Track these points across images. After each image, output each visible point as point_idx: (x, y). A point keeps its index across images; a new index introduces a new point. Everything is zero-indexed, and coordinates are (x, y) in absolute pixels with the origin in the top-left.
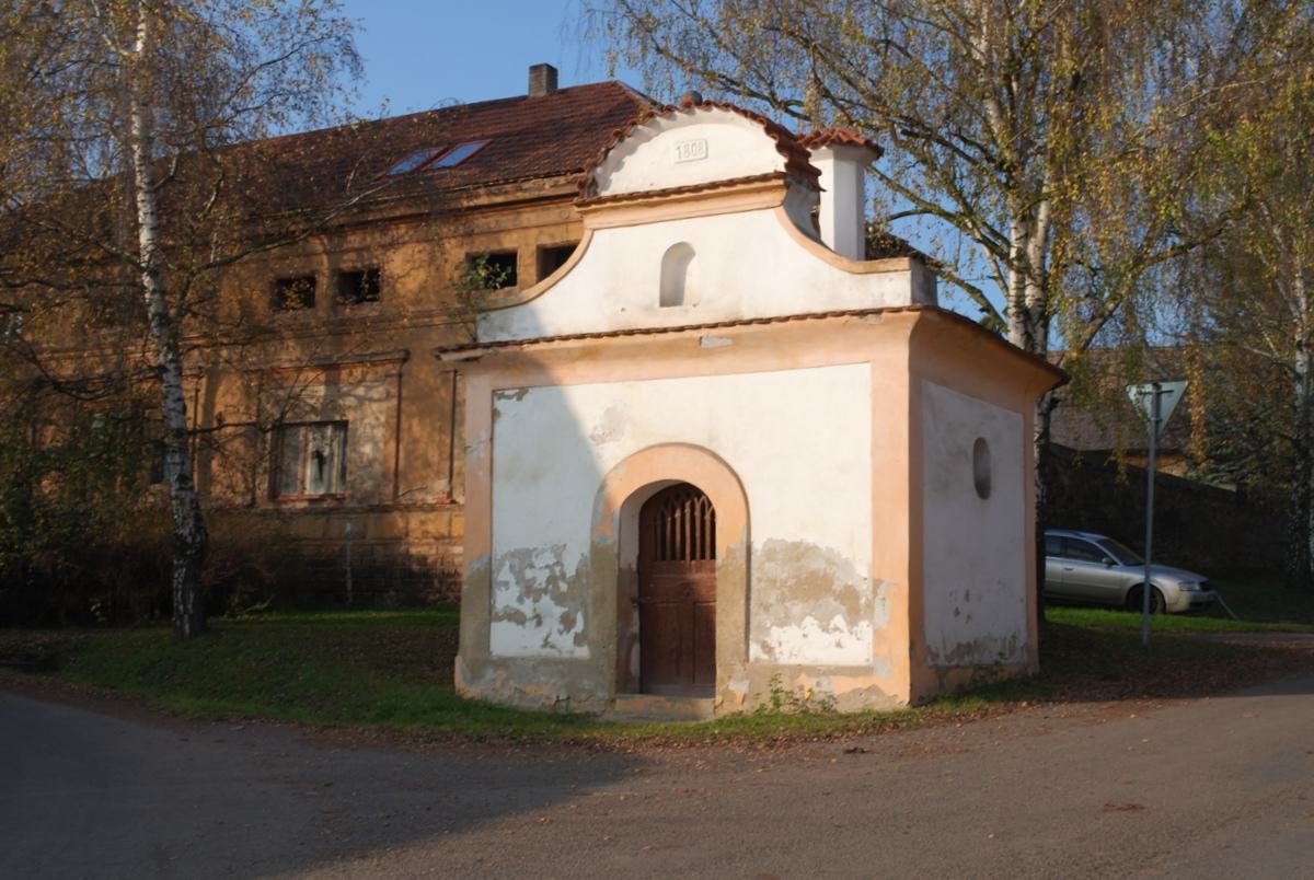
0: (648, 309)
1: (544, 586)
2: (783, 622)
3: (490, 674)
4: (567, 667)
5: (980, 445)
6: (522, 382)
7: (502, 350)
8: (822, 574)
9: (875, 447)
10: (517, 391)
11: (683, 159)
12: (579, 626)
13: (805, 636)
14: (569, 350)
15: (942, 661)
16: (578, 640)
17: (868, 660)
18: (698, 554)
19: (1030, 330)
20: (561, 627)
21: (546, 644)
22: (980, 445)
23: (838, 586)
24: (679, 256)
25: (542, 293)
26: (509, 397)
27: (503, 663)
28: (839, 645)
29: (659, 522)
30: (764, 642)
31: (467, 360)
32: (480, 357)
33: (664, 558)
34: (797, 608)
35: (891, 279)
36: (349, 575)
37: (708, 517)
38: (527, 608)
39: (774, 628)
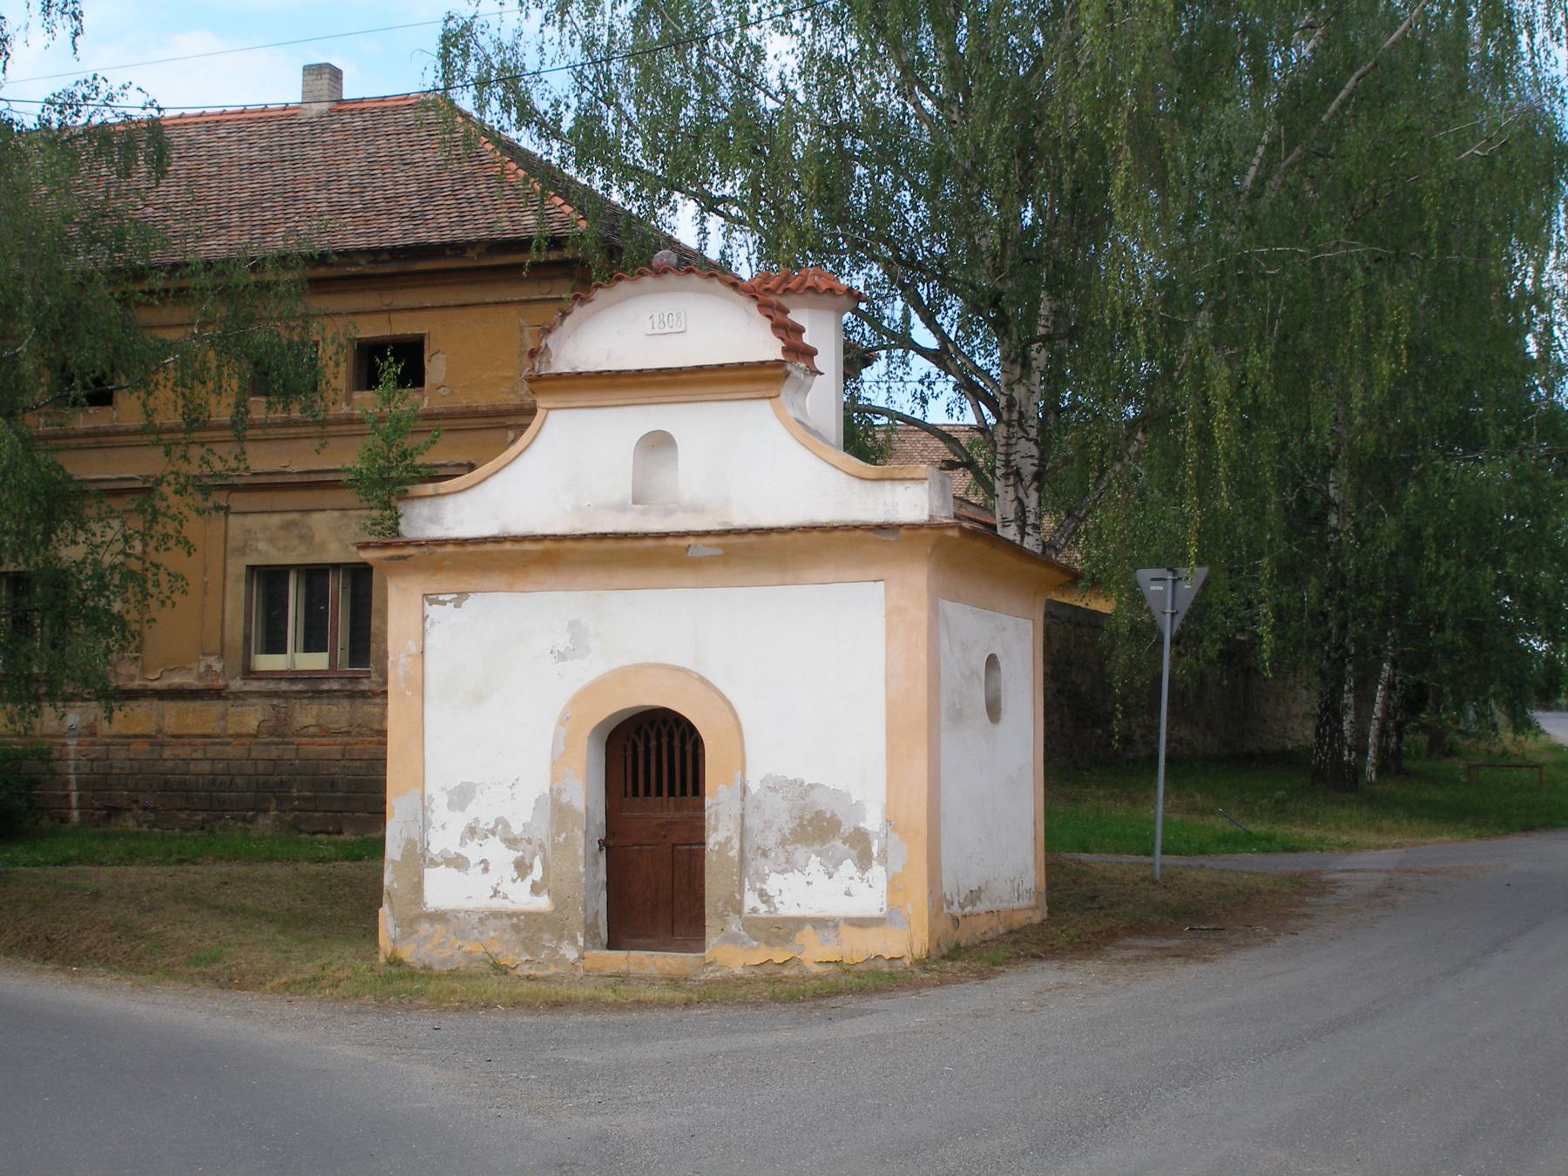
0: (621, 508)
1: (491, 826)
2: (788, 866)
3: (424, 928)
4: (527, 926)
5: (992, 662)
6: (461, 587)
7: (440, 550)
10: (456, 596)
11: (657, 331)
14: (525, 553)
15: (956, 909)
16: (536, 889)
17: (881, 909)
19: (1021, 495)
20: (515, 875)
21: (496, 893)
22: (992, 662)
23: (847, 828)
24: (658, 443)
25: (484, 480)
26: (443, 603)
27: (439, 917)
28: (848, 894)
29: (630, 753)
30: (762, 890)
31: (391, 558)
32: (411, 556)
33: (635, 794)
34: (800, 852)
35: (906, 488)
36: (73, 786)
37: (689, 747)
38: (472, 851)
39: (773, 874)
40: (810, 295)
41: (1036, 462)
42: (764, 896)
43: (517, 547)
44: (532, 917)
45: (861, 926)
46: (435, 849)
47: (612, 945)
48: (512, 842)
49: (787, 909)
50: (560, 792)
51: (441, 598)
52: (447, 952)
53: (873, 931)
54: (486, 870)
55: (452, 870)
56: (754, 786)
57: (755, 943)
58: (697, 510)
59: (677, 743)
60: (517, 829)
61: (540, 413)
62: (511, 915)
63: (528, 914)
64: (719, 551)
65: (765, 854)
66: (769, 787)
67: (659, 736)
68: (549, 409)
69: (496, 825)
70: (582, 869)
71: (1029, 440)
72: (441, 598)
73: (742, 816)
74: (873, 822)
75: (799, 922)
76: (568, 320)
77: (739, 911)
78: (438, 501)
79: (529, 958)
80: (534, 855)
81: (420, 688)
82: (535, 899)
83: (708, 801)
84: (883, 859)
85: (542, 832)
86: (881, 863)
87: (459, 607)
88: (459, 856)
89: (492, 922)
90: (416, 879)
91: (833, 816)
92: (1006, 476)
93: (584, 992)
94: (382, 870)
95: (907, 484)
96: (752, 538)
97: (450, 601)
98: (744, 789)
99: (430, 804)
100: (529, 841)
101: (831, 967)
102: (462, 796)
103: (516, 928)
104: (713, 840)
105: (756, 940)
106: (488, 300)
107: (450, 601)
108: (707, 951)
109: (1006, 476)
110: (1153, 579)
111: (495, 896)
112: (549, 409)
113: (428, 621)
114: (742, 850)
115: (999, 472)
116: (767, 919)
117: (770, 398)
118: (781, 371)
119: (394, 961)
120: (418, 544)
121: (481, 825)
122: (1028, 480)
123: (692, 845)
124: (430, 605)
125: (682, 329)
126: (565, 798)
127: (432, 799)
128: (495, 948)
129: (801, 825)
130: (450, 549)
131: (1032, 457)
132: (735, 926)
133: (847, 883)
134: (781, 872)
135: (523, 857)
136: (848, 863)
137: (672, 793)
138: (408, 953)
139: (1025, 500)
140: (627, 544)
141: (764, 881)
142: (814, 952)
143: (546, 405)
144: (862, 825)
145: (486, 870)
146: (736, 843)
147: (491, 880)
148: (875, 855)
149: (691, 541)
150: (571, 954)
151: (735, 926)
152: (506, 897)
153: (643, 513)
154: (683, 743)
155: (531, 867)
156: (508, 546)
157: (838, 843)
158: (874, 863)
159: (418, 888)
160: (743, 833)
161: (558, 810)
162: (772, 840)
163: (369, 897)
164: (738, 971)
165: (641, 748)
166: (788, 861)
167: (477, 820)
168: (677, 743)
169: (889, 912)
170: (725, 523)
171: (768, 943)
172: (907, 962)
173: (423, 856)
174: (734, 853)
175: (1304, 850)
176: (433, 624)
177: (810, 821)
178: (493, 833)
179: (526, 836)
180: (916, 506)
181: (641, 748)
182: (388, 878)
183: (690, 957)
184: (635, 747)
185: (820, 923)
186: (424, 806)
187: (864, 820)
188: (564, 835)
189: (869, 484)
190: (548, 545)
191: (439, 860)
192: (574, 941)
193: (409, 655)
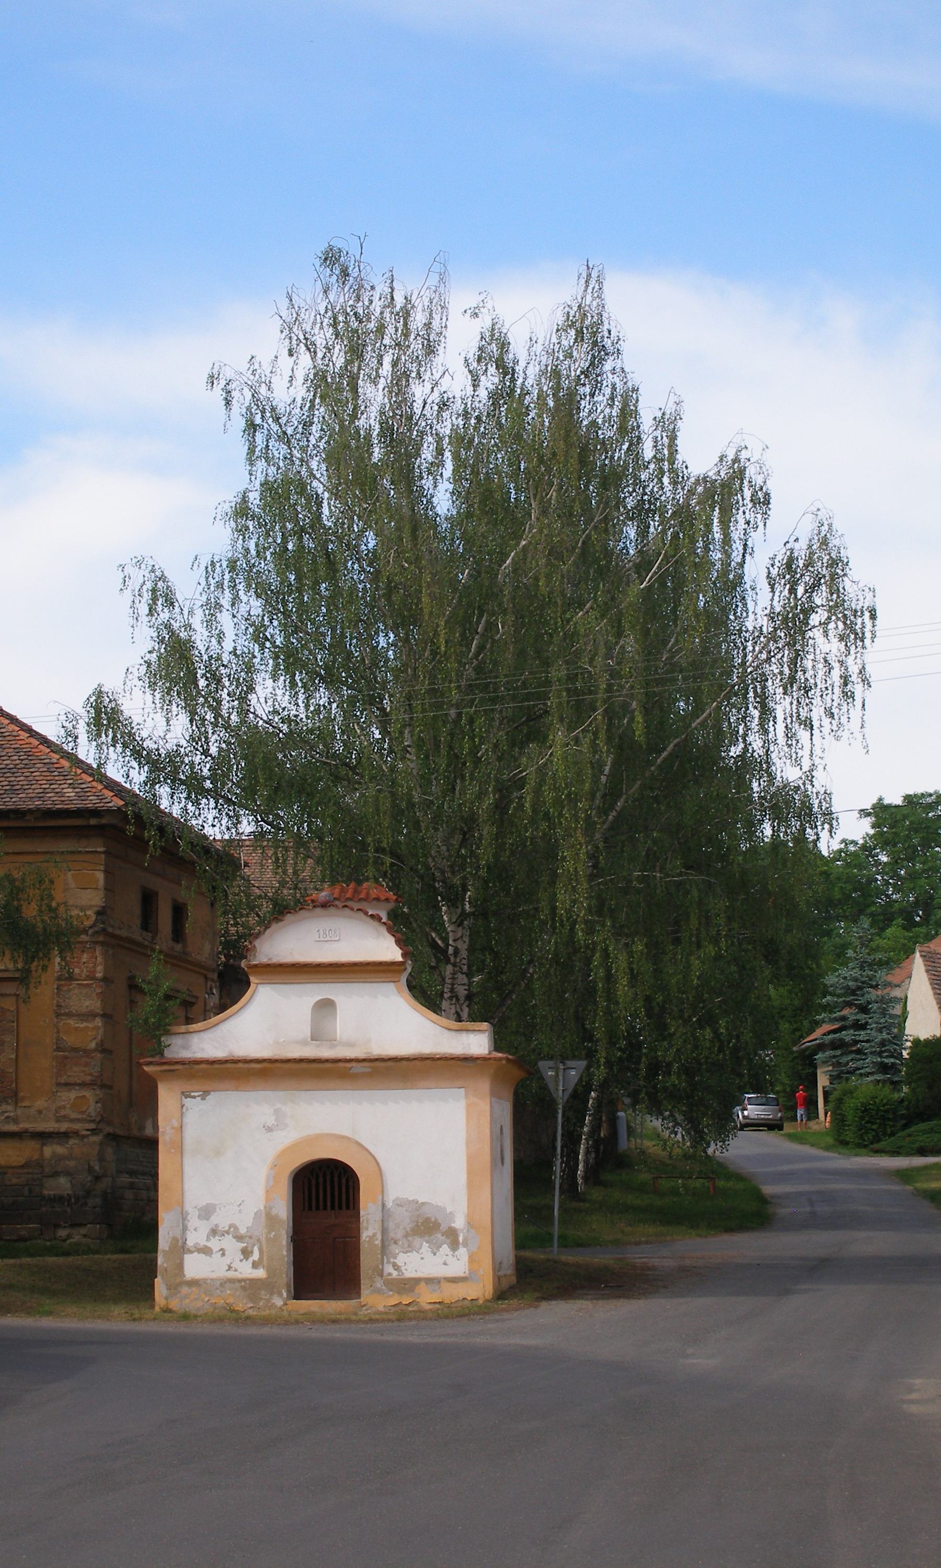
0: (304, 1043)
1: (227, 1228)
2: (410, 1249)
3: (185, 1290)
4: (250, 1287)
7: (196, 1067)
8: (433, 1220)
9: (468, 1144)
11: (321, 939)
12: (256, 1256)
13: (422, 1258)
16: (255, 1265)
17: (465, 1272)
18: (337, 1205)
19: (459, 1010)
20: (242, 1257)
21: (230, 1268)
23: (444, 1227)
24: (326, 1006)
26: (194, 1097)
27: (194, 1283)
30: (394, 1262)
31: (165, 1071)
32: (176, 1070)
33: (310, 1208)
34: (417, 1241)
38: (215, 1244)
39: (401, 1254)
40: (375, 902)
41: (467, 988)
42: (396, 1267)
43: (246, 1066)
44: (253, 1282)
45: (453, 1282)
46: (190, 1243)
47: (297, 1296)
48: (239, 1238)
49: (409, 1274)
50: (271, 1208)
51: (192, 1094)
52: (200, 1304)
53: (460, 1284)
54: (223, 1254)
55: (202, 1256)
56: (389, 1204)
57: (391, 1293)
58: (350, 1045)
59: (336, 1179)
60: (243, 1231)
61: (252, 986)
62: (240, 1281)
63: (252, 1280)
64: (370, 1070)
65: (396, 1243)
66: (398, 1204)
67: (325, 1175)
68: (258, 984)
69: (230, 1228)
70: (285, 1253)
71: (463, 973)
72: (193, 1094)
73: (382, 1221)
74: (459, 1223)
75: (417, 1281)
76: (268, 931)
77: (381, 1275)
78: (186, 1036)
79: (252, 1305)
80: (254, 1245)
81: (180, 1148)
82: (255, 1271)
83: (362, 1213)
84: (465, 1244)
85: (260, 1231)
86: (464, 1247)
87: (205, 1099)
88: (206, 1247)
89: (228, 1285)
90: (178, 1261)
91: (436, 1220)
92: (451, 998)
93: (343, 1317)
94: (156, 1258)
95: (476, 1033)
96: (390, 1064)
97: (199, 1096)
98: (383, 1205)
99: (186, 1217)
100: (251, 1237)
101: (437, 1306)
102: (207, 1212)
103: (244, 1288)
104: (365, 1235)
105: (391, 1291)
106: (39, 850)
107: (199, 1096)
108: (362, 1298)
109: (451, 998)
110: (550, 1068)
111: (229, 1270)
112: (258, 984)
113: (184, 1108)
114: (382, 1240)
115: (446, 996)
116: (398, 1279)
117: (394, 982)
118: (403, 968)
119: (167, 1310)
120: (182, 1062)
121: (220, 1229)
122: (462, 999)
123: (345, 1238)
124: (186, 1098)
125: (337, 938)
126: (274, 1212)
127: (187, 1214)
128: (231, 1301)
129: (417, 1226)
130: (203, 1066)
131: (464, 984)
132: (379, 1283)
133: (445, 1258)
134: (406, 1252)
135: (246, 1247)
136: (445, 1246)
137: (333, 1208)
138: (174, 1304)
139: (461, 1013)
140: (321, 1066)
141: (395, 1258)
142: (426, 1298)
143: (257, 981)
144: (453, 1225)
145: (223, 1254)
146: (379, 1236)
147: (227, 1260)
148: (461, 1242)
149: (354, 1064)
150: (279, 1302)
151: (379, 1283)
152: (236, 1270)
153: (318, 1046)
154: (347, 1182)
155: (252, 1252)
156: (240, 1065)
157: (439, 1236)
158: (461, 1246)
159: (180, 1266)
160: (384, 1231)
161: (271, 1220)
162: (399, 1234)
163: (151, 1270)
164: (381, 1308)
165: (314, 1182)
166: (409, 1246)
167: (217, 1225)
168: (336, 1179)
169: (470, 1273)
170: (368, 1053)
171: (399, 1293)
172: (481, 1302)
173: (183, 1247)
174: (378, 1242)
175: (589, 1245)
176: (187, 1109)
177: (423, 1223)
178: (228, 1232)
179: (248, 1234)
180: (481, 1045)
181: (314, 1182)
182: (160, 1260)
183: (353, 1302)
184: (310, 1181)
185: (429, 1281)
186: (184, 1217)
187: (454, 1222)
188: (273, 1233)
189: (453, 1033)
190: (266, 1065)
191: (193, 1249)
192: (281, 1295)
193: (173, 1128)
